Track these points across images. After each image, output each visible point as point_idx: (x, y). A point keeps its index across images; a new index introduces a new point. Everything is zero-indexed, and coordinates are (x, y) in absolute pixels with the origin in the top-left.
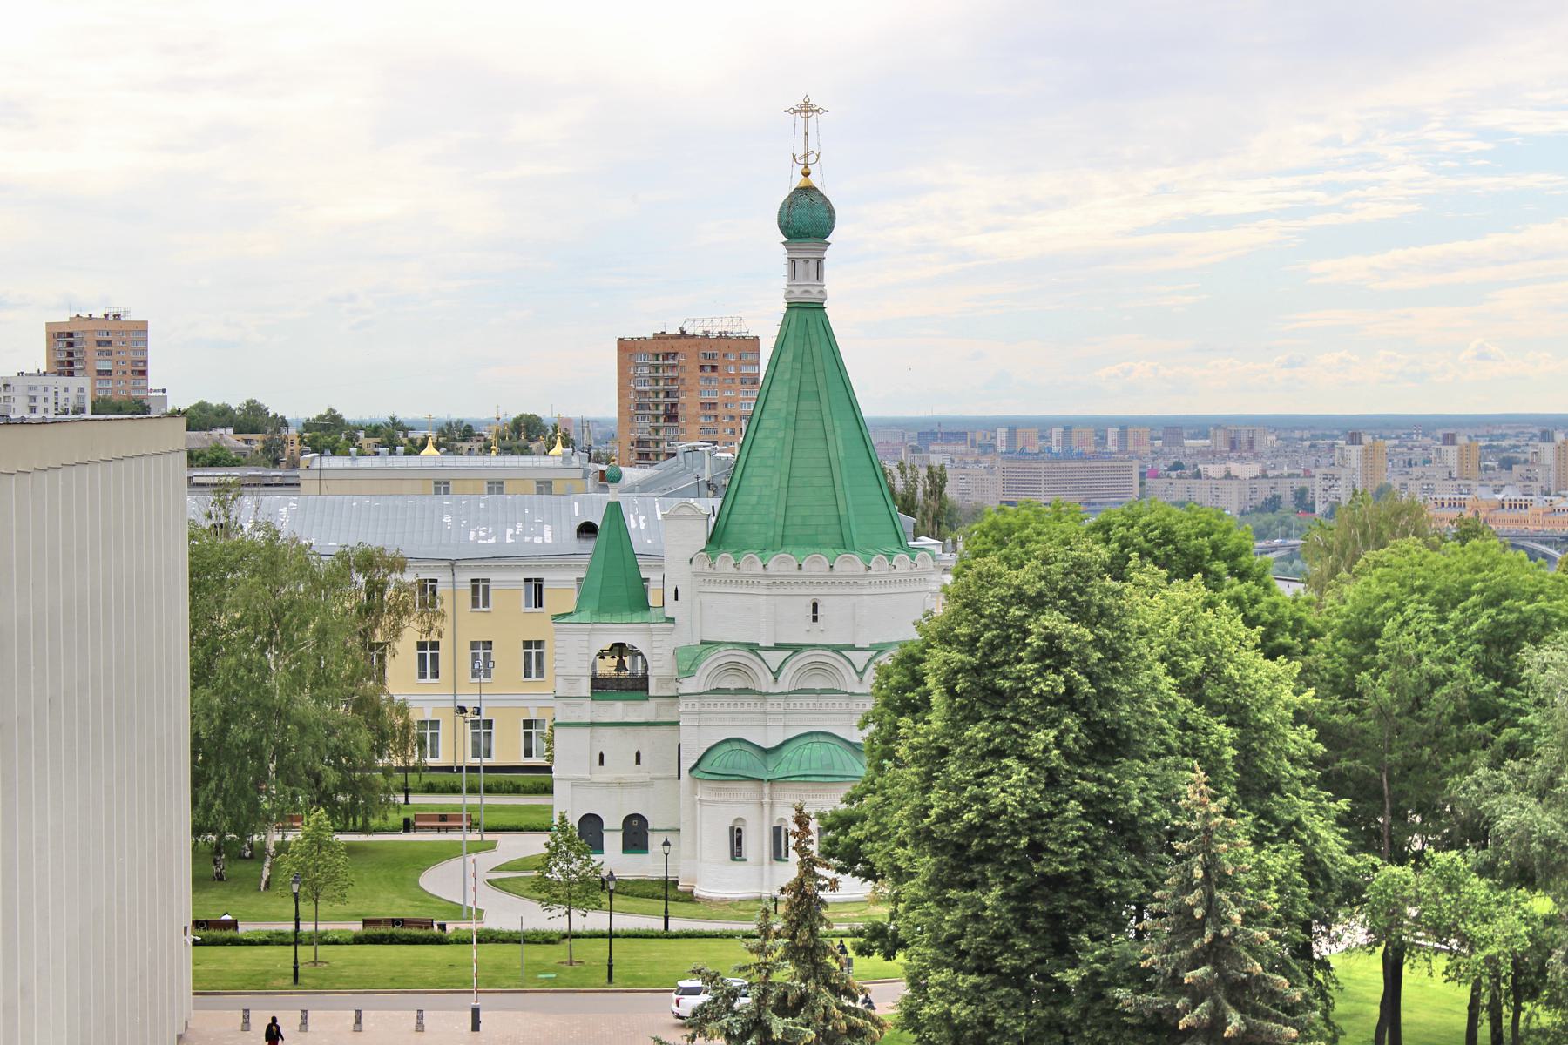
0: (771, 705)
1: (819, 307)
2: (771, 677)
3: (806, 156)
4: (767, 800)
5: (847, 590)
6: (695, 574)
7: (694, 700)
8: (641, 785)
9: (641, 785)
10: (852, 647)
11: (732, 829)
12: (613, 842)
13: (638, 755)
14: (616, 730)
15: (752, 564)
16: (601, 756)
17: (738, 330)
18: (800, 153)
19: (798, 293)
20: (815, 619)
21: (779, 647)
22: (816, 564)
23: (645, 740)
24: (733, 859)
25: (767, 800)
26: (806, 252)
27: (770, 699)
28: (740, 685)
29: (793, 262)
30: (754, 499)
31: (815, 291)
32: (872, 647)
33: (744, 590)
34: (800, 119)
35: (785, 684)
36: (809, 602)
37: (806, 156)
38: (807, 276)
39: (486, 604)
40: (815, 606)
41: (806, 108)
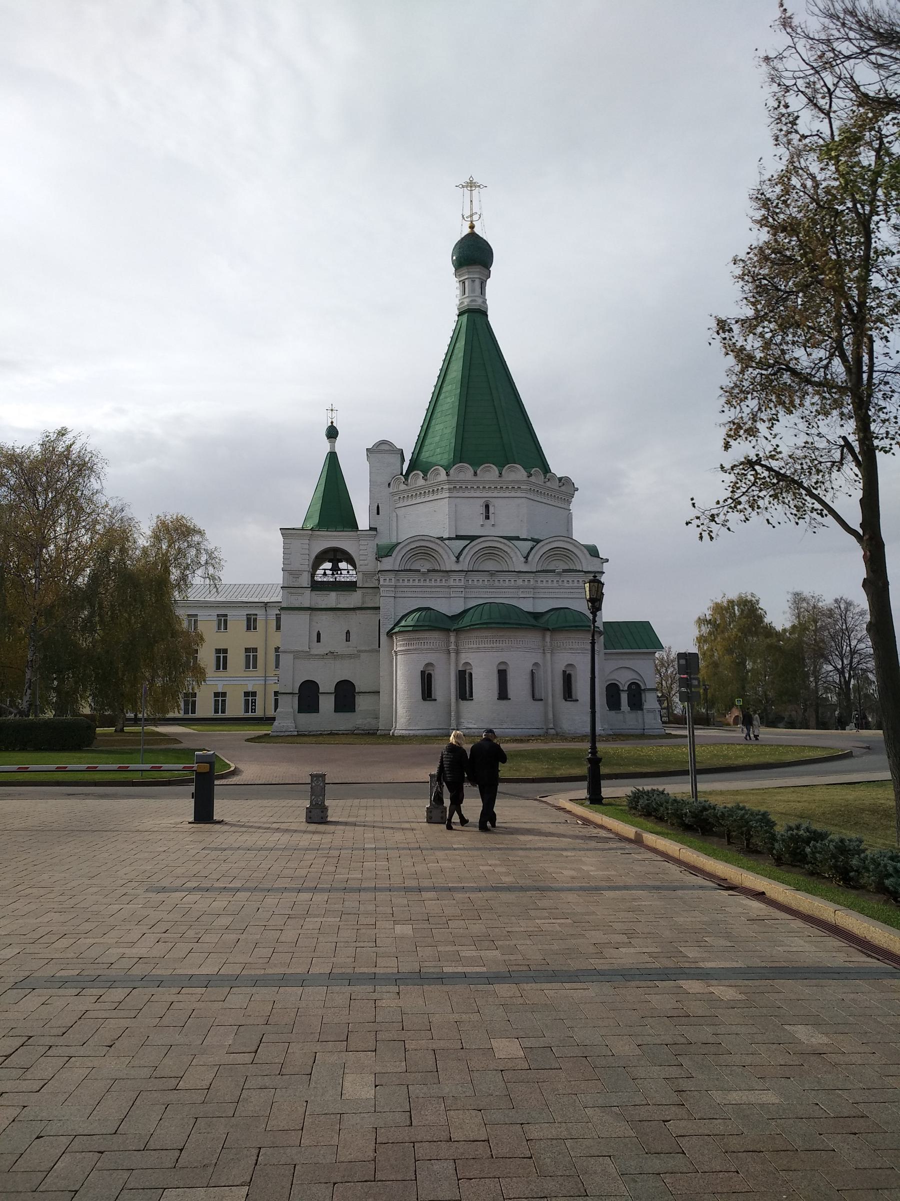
0: (455, 581)
1: (484, 314)
2: (523, 559)
3: (471, 216)
4: (453, 646)
5: (513, 494)
6: (393, 494)
7: (391, 576)
8: (350, 656)
9: (350, 656)
10: (517, 538)
11: (423, 673)
12: (327, 703)
13: (348, 632)
16: (319, 634)
17: (341, 714)
18: (467, 213)
20: (487, 518)
21: (459, 538)
22: (490, 473)
23: (355, 622)
24: (424, 699)
25: (453, 646)
27: (454, 576)
30: (437, 439)
31: (480, 301)
32: (533, 540)
34: (467, 191)
35: (464, 565)
36: (481, 502)
37: (471, 216)
40: (487, 507)
41: (471, 185)
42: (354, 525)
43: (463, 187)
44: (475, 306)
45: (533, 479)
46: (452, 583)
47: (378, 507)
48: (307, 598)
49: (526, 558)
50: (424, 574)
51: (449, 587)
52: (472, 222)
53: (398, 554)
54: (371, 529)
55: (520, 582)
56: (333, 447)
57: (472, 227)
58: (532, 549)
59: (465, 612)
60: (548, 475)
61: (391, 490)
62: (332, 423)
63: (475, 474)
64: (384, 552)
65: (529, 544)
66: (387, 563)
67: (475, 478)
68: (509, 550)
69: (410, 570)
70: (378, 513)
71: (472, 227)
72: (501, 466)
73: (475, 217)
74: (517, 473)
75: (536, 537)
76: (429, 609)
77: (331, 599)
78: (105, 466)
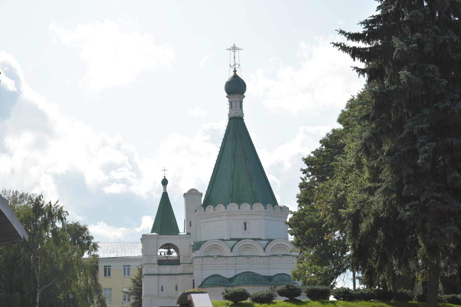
2: (263, 250)
3: (235, 65)
7: (200, 259)
10: (260, 239)
13: (176, 286)
14: (167, 277)
15: (221, 208)
16: (162, 287)
18: (232, 64)
19: (232, 115)
20: (245, 229)
21: (232, 239)
22: (246, 207)
26: (236, 98)
27: (230, 259)
28: (217, 254)
29: (231, 103)
32: (268, 240)
33: (217, 219)
34: (232, 53)
35: (235, 253)
36: (242, 222)
37: (235, 65)
38: (236, 107)
39: (109, 275)
40: (245, 224)
41: (234, 48)
42: (178, 231)
43: (230, 50)
44: (237, 115)
45: (267, 210)
46: (228, 262)
47: (190, 223)
48: (156, 269)
49: (264, 249)
50: (215, 258)
51: (227, 264)
52: (235, 69)
53: (203, 247)
54: (188, 234)
55: (261, 261)
56: (165, 189)
57: (235, 71)
58: (267, 244)
59: (236, 276)
60: (276, 206)
61: (197, 213)
62: (165, 177)
63: (239, 208)
64: (197, 246)
65: (266, 242)
66: (198, 253)
67: (239, 210)
68: (255, 245)
69: (208, 256)
70: (190, 226)
71: (235, 71)
72: (252, 204)
73: (237, 66)
74: (259, 207)
75: (269, 238)
76: (218, 276)
77: (167, 269)
78: (67, 215)
